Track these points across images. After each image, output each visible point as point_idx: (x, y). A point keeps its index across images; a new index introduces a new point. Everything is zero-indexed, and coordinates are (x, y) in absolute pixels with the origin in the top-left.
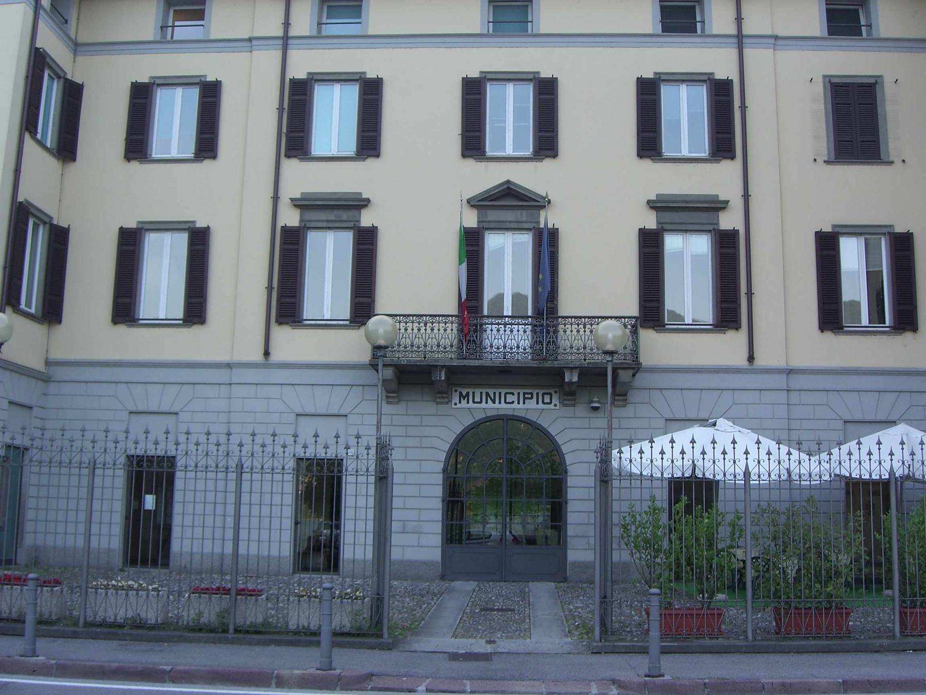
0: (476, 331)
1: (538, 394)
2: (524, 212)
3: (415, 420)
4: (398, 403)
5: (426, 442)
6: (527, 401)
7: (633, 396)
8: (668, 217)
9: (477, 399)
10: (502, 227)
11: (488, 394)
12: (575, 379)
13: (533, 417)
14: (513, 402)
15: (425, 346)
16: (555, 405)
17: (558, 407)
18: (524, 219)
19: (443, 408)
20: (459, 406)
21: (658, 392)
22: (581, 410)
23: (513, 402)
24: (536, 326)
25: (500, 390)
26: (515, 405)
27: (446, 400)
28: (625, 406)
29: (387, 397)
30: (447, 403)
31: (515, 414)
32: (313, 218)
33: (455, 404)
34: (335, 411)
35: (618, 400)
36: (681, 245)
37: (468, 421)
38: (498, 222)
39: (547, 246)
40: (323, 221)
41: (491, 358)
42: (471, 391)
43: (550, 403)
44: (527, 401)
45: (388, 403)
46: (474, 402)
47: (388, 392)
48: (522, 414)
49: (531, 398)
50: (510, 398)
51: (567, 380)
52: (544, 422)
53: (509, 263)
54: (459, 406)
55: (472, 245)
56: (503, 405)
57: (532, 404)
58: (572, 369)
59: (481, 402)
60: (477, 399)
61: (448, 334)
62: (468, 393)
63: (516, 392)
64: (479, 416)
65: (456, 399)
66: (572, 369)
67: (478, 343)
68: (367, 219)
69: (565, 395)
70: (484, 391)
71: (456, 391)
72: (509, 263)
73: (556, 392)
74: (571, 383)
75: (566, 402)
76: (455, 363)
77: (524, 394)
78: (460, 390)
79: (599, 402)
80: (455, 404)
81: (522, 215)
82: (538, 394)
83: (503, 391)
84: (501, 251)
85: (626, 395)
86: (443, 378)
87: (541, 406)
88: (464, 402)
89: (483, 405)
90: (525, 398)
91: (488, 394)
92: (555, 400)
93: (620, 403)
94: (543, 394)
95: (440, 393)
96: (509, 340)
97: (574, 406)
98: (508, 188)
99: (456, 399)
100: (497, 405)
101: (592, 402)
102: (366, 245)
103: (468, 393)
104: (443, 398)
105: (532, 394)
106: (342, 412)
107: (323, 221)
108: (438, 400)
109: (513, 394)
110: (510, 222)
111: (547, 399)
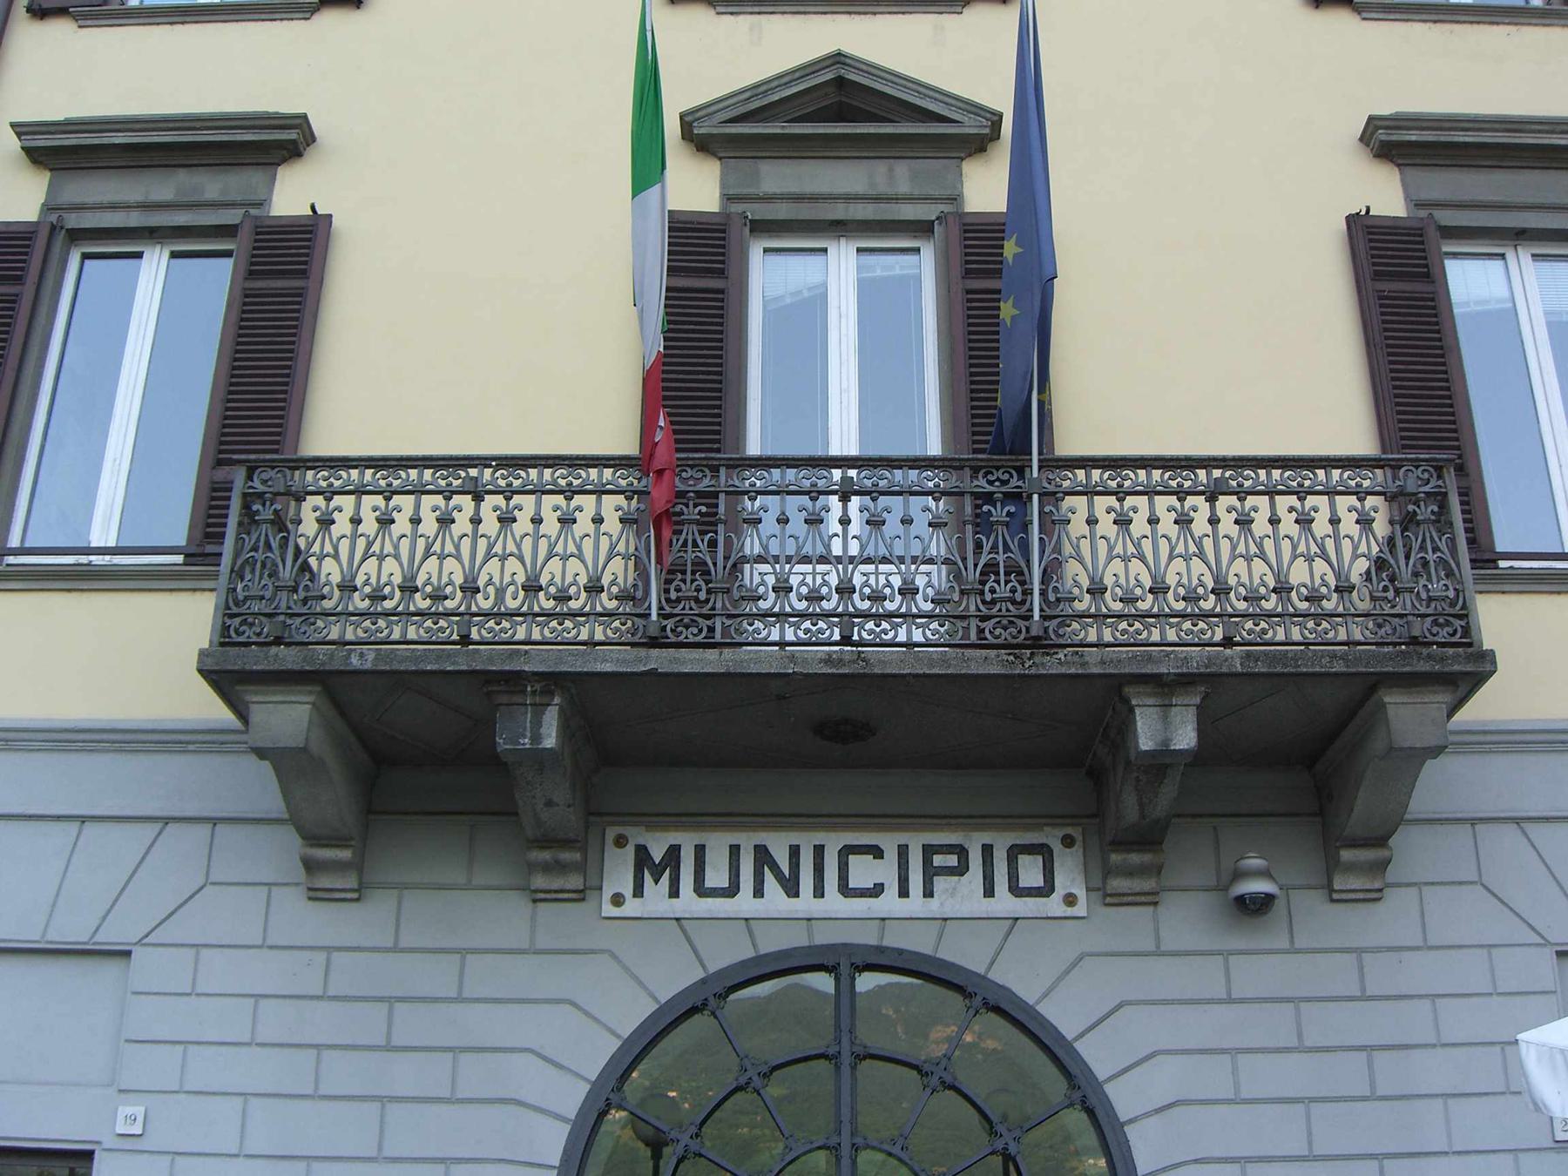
0: (708, 523)
1: (987, 851)
2: (902, 169)
3: (435, 976)
4: (359, 894)
5: (476, 1075)
6: (940, 883)
7: (1413, 851)
8: (1443, 183)
9: (717, 877)
10: (816, 226)
11: (763, 857)
12: (1185, 737)
13: (967, 953)
14: (877, 890)
15: (470, 589)
16: (1070, 900)
17: (1080, 909)
18: (904, 188)
19: (559, 921)
20: (632, 907)
21: (1511, 828)
22: (1185, 918)
23: (877, 890)
24: (988, 498)
25: (819, 837)
26: (889, 903)
27: (574, 881)
28: (1373, 897)
29: (310, 866)
30: (580, 895)
31: (890, 941)
32: (90, 199)
33: (618, 900)
34: (72, 931)
35: (1352, 868)
36: (1500, 291)
37: (674, 976)
38: (798, 198)
39: (997, 298)
40: (127, 207)
41: (778, 642)
42: (687, 841)
43: (1047, 890)
44: (940, 883)
45: (316, 895)
46: (701, 890)
47: (312, 838)
48: (919, 942)
49: (961, 870)
50: (863, 871)
51: (1146, 742)
52: (1021, 977)
53: (844, 348)
54: (632, 907)
55: (699, 281)
56: (834, 902)
57: (961, 896)
58: (1165, 686)
59: (732, 890)
60: (717, 877)
61: (593, 545)
62: (674, 853)
63: (889, 842)
64: (727, 952)
65: (619, 876)
66: (1165, 686)
67: (719, 573)
68: (290, 194)
69: (1120, 844)
70: (748, 841)
71: (621, 842)
72: (844, 348)
73: (1068, 842)
74: (1161, 762)
75: (1118, 884)
76: (607, 662)
77: (929, 851)
78: (637, 836)
79: (1265, 874)
80: (618, 900)
81: (899, 176)
82: (987, 851)
83: (834, 842)
84: (808, 313)
85: (1381, 841)
86: (550, 742)
87: (1005, 903)
88: (656, 891)
89: (745, 902)
90: (930, 872)
91: (763, 857)
92: (1069, 877)
93: (1355, 882)
94: (1014, 853)
95: (545, 842)
96: (854, 576)
97: (1150, 899)
98: (840, 82)
99: (619, 876)
100: (806, 903)
101: (1239, 875)
102: (280, 283)
103: (674, 853)
104: (559, 868)
105: (962, 852)
106: (110, 936)
107: (127, 207)
108: (539, 881)
109: (877, 852)
110: (849, 198)
111: (1031, 873)
